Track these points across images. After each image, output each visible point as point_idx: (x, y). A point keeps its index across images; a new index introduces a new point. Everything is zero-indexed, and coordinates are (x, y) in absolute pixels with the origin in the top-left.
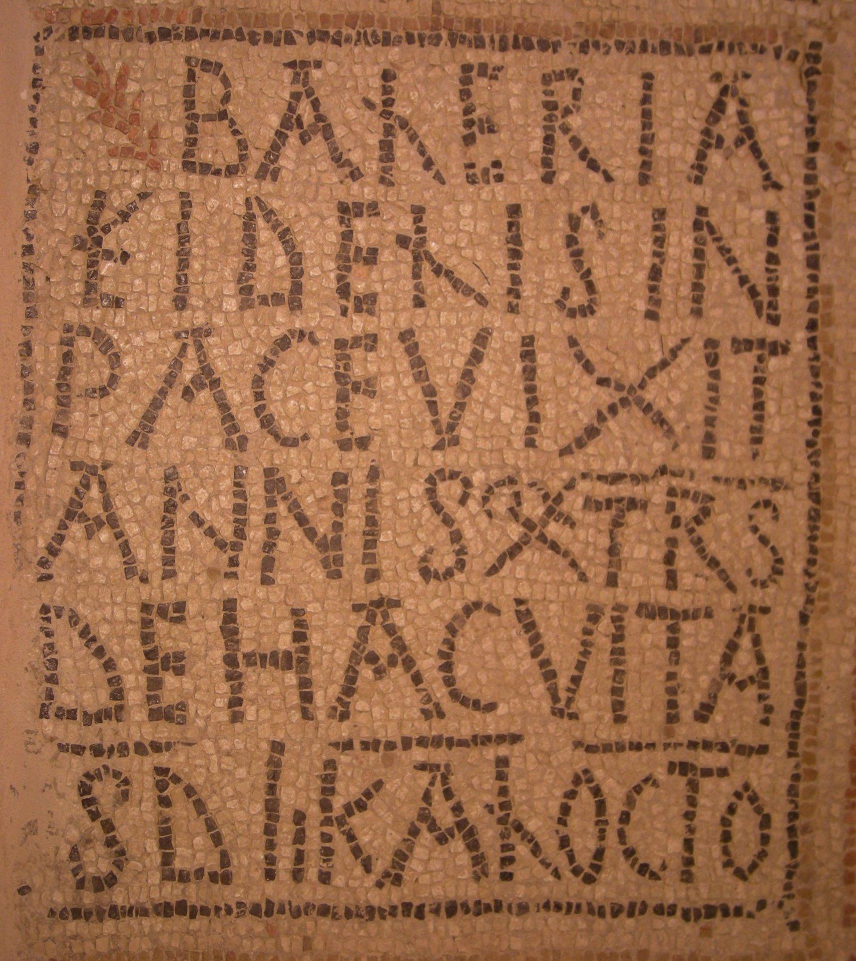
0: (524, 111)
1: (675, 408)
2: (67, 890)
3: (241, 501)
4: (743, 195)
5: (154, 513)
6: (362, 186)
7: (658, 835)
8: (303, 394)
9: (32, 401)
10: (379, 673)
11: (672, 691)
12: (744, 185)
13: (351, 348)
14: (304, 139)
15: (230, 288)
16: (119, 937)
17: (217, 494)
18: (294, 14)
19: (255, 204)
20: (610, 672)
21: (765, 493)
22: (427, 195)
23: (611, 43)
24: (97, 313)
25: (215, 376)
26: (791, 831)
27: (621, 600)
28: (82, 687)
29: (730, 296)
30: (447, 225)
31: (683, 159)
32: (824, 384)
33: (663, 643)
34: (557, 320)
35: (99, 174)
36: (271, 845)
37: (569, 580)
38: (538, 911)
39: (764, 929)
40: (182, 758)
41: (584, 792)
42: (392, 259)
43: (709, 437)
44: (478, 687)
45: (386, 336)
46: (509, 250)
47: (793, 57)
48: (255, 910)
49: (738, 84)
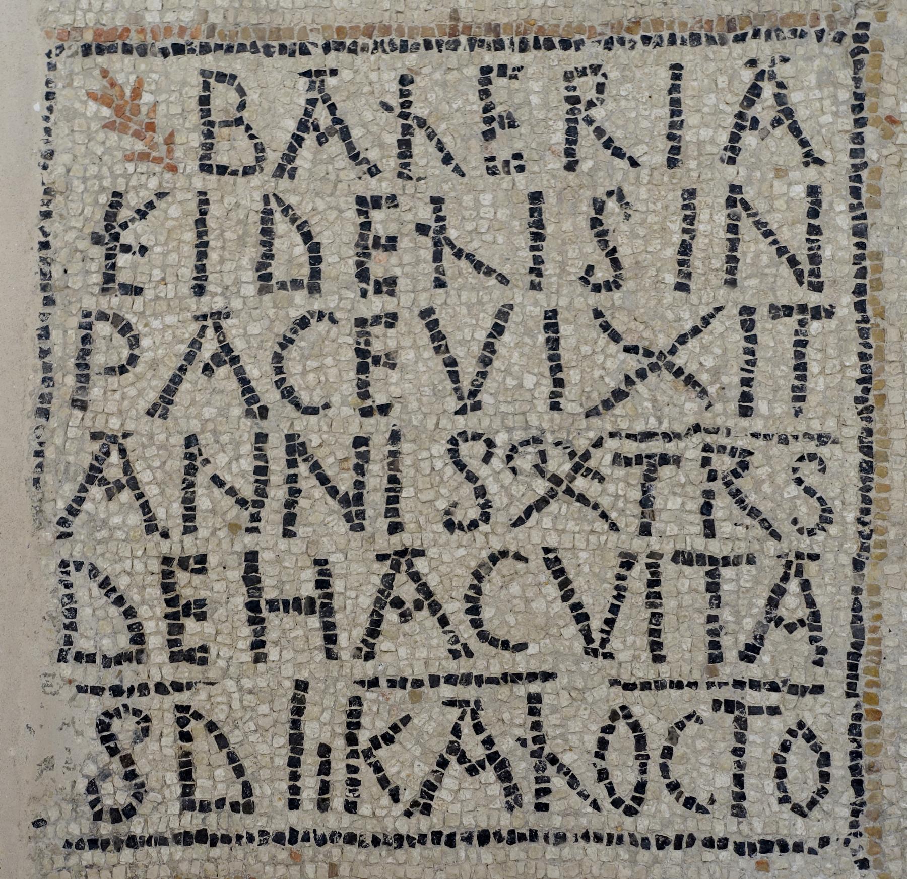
0: (545, 105)
1: (708, 371)
2: (84, 821)
3: (262, 464)
4: (780, 172)
5: (174, 476)
6: (380, 181)
7: (704, 769)
8: (324, 367)
9: (51, 379)
10: (405, 617)
11: (714, 633)
12: (781, 163)
13: (372, 325)
14: (322, 140)
15: (250, 275)
16: (136, 866)
17: (238, 458)
18: (309, 28)
19: (272, 200)
20: (647, 614)
21: (811, 447)
22: (446, 187)
23: (637, 38)
24: (115, 301)
25: (235, 353)
26: (855, 770)
27: (656, 547)
28: (101, 631)
29: (768, 266)
30: (467, 214)
31: (713, 141)
32: (874, 345)
33: (703, 588)
34: (581, 295)
35: (115, 177)
36: (294, 777)
37: (598, 530)
38: (577, 841)
39: (829, 866)
40: (203, 695)
41: (622, 726)
42: (411, 245)
43: (746, 397)
44: (506, 629)
45: (404, 315)
46: (532, 233)
48: (279, 838)
49: (775, 69)
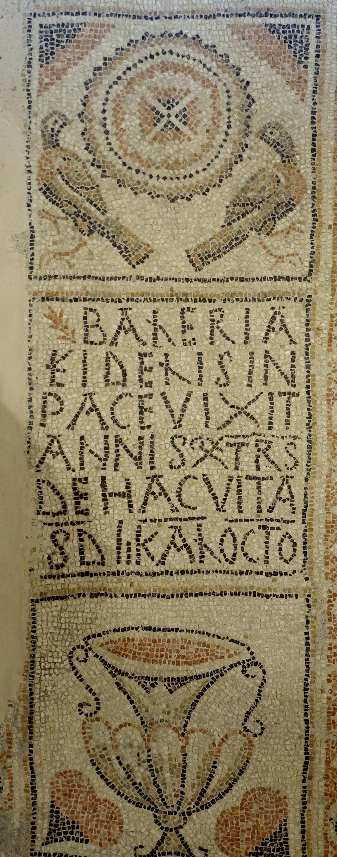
0: (203, 322)
4: (282, 346)
8: (128, 412)
10: (156, 498)
14: (126, 332)
15: (102, 380)
20: (237, 497)
21: (291, 440)
23: (234, 299)
26: (304, 548)
27: (240, 474)
31: (260, 335)
35: (54, 345)
36: (119, 553)
40: (87, 526)
41: (228, 534)
43: (270, 423)
47: (301, 300)
48: (114, 574)
